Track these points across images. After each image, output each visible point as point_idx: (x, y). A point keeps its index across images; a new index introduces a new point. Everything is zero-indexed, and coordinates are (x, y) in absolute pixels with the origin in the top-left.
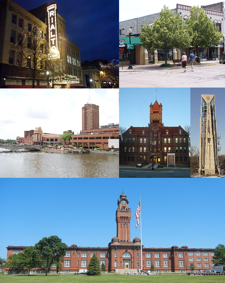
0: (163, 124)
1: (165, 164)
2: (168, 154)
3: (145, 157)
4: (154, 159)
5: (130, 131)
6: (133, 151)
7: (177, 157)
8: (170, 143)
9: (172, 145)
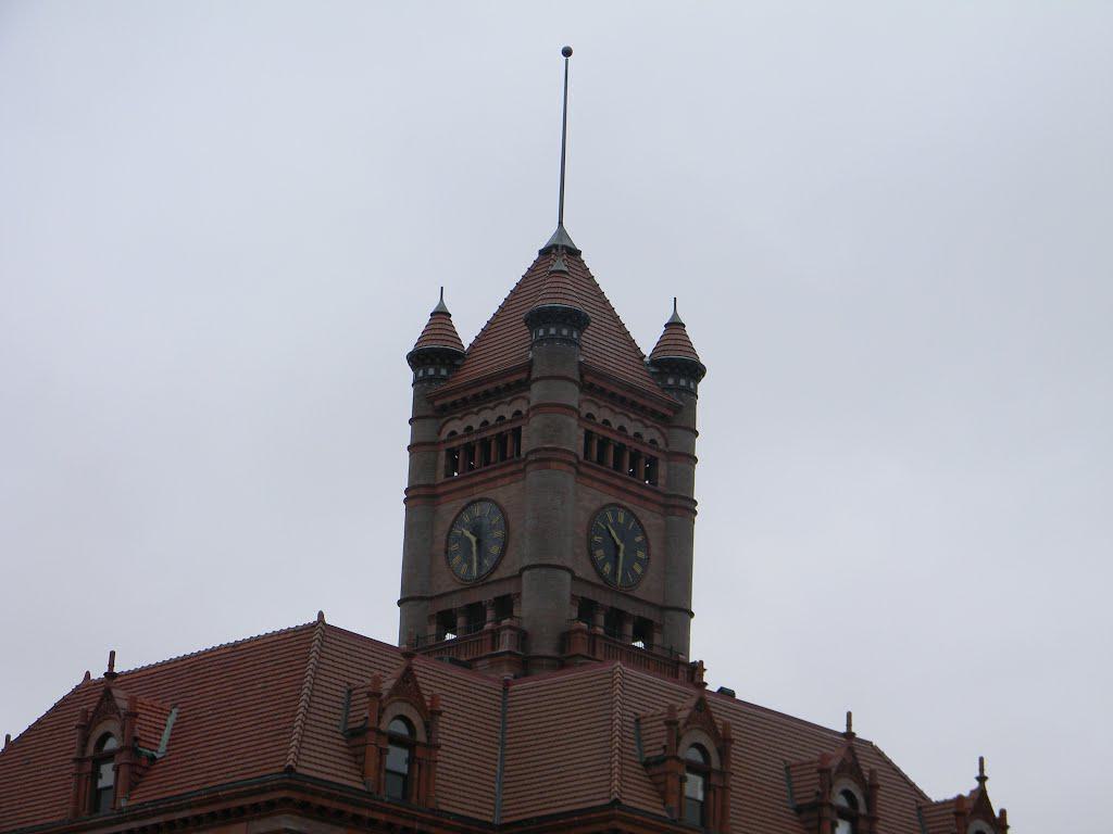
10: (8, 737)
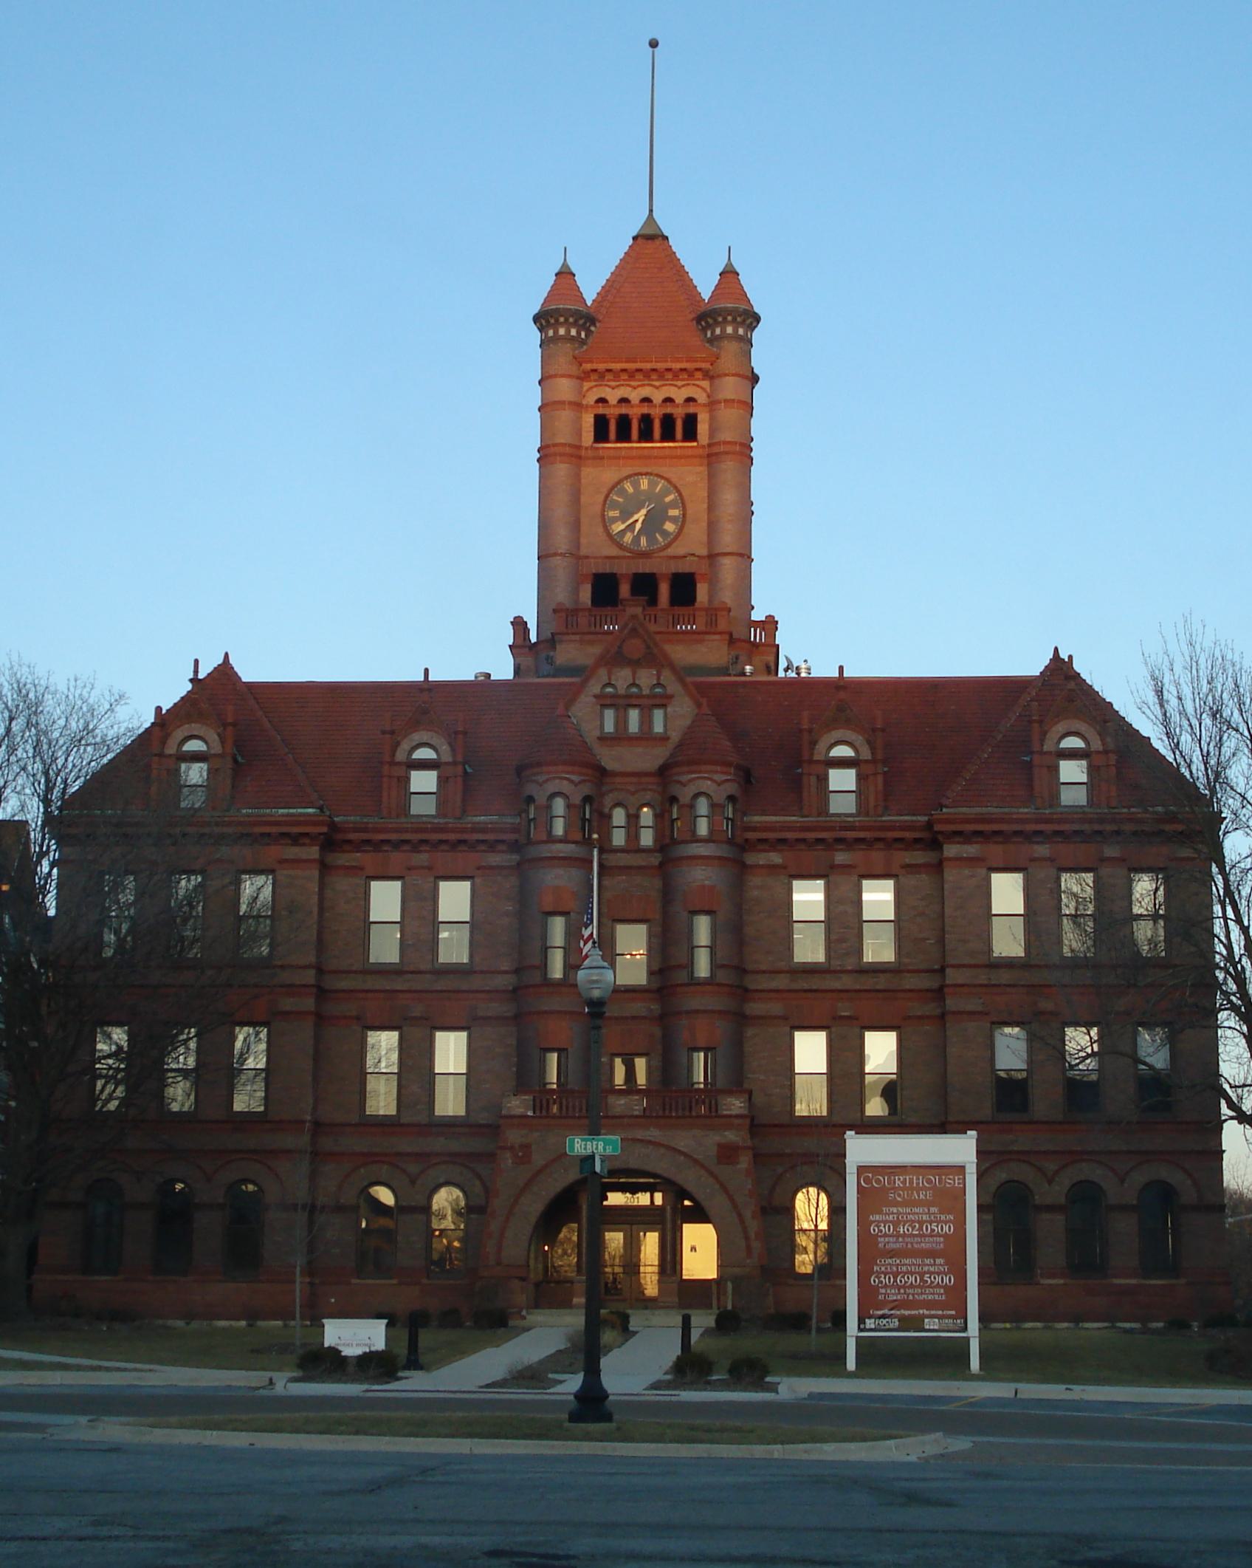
0: (770, 624)
1: (798, 1322)
2: (862, 1150)
3: (445, 1199)
4: (615, 1239)
5: (196, 757)
6: (247, 1099)
7: (1006, 1208)
8: (819, 956)
9: (933, 989)
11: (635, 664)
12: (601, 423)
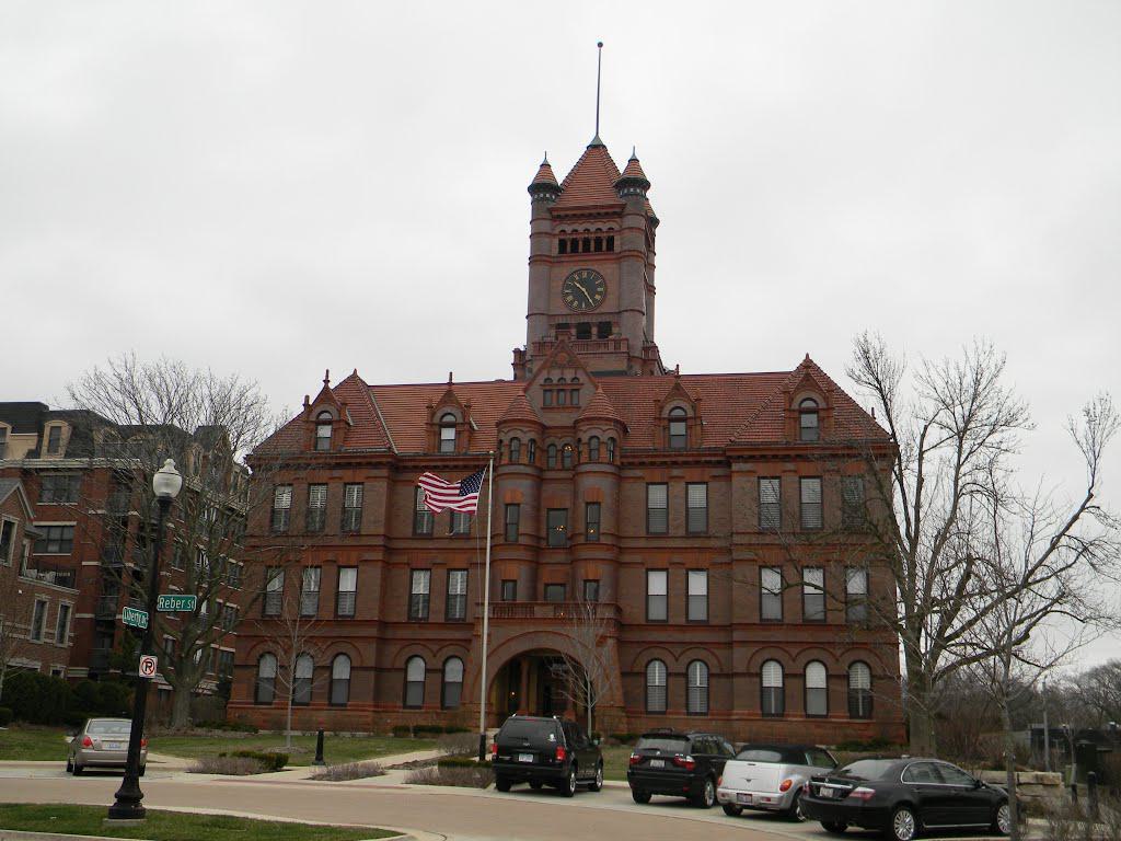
10: (307, 398)
11: (562, 367)
12: (562, 244)
